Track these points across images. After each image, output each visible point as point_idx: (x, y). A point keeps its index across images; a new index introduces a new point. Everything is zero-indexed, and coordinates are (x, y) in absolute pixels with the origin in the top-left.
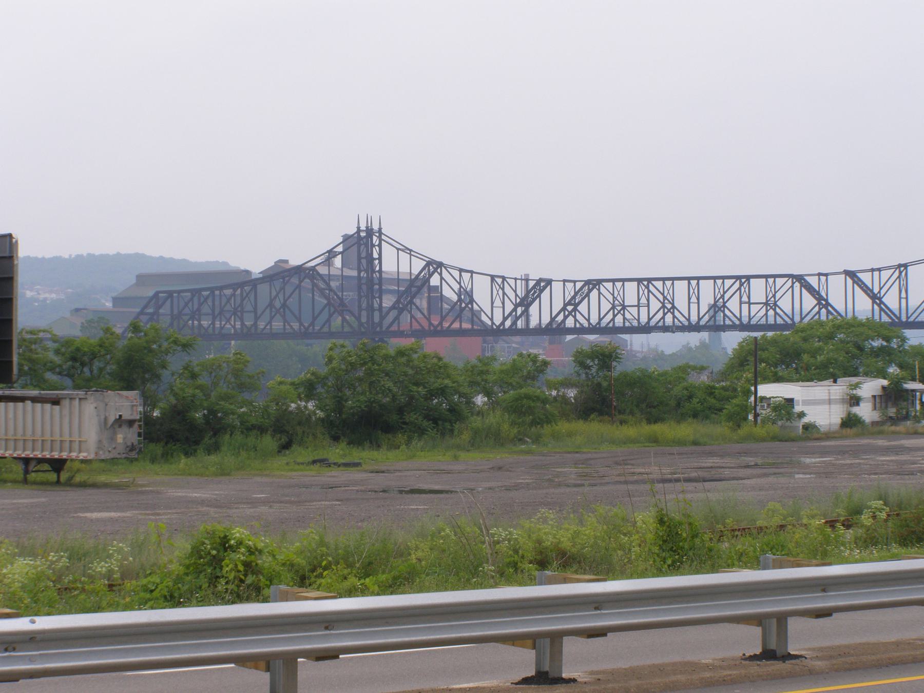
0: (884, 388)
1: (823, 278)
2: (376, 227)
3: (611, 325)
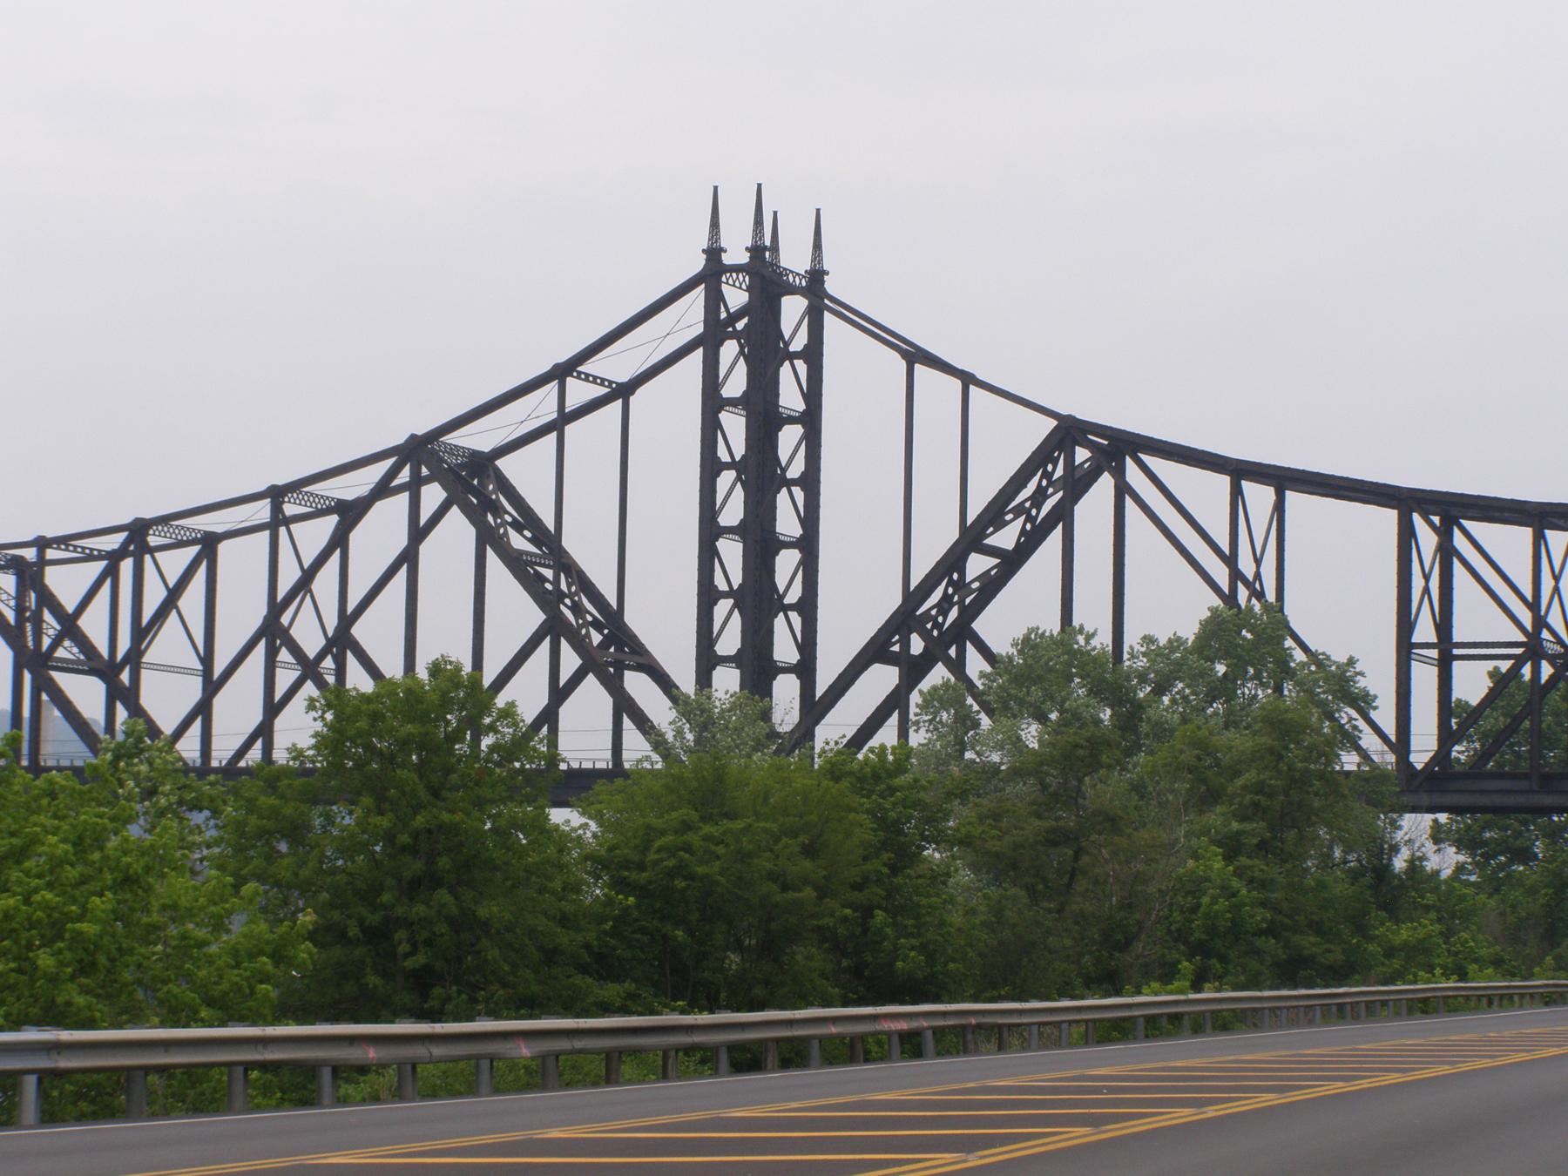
0: (458, 668)
1: (1259, 496)
2: (794, 258)
3: (952, 652)
